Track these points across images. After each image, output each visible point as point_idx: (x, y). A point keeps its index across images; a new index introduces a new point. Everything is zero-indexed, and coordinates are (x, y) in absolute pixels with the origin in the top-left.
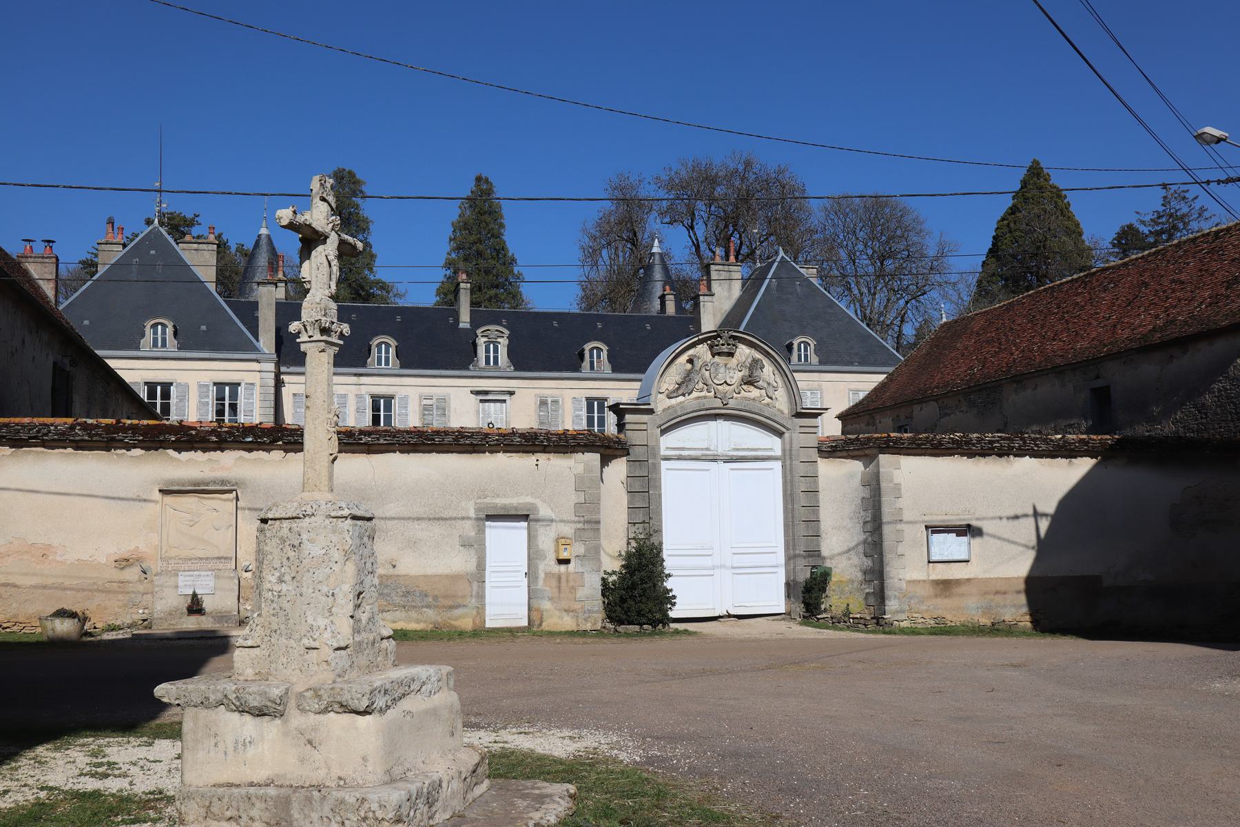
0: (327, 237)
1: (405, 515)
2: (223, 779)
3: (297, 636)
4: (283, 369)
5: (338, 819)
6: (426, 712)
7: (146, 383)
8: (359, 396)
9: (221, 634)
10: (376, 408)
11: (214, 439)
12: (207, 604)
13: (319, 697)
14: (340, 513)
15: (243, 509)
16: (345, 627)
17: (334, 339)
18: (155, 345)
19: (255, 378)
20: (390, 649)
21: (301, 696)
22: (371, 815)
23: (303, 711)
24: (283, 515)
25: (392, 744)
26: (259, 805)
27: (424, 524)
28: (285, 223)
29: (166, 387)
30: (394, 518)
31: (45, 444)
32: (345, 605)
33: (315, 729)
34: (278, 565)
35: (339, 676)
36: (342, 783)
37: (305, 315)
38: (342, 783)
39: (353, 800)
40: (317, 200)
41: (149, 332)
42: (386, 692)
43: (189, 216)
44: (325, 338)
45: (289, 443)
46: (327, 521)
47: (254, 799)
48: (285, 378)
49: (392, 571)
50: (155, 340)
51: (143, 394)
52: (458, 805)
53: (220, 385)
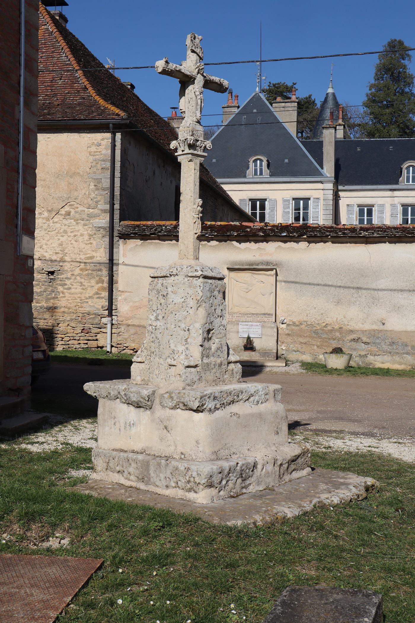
0: (195, 79)
1: (392, 287)
2: (118, 446)
3: (164, 357)
4: (340, 187)
5: (175, 480)
6: (252, 415)
7: (250, 200)
8: (393, 206)
9: (260, 364)
10: (361, 212)
11: (262, 234)
12: (257, 344)
13: (172, 398)
14: (194, 274)
15: (281, 281)
16: (196, 353)
17: (200, 153)
18: (256, 174)
19: (319, 194)
20: (235, 370)
21: (162, 396)
22: (192, 479)
23: (163, 407)
24: (159, 275)
25: (218, 433)
26: (133, 465)
27: (405, 295)
28: (160, 70)
29: (263, 202)
30: (384, 290)
31: (159, 238)
32: (197, 338)
33: (169, 419)
34: (155, 309)
35: (189, 385)
36: (183, 457)
37: (180, 137)
38: (183, 457)
39: (182, 468)
40: (189, 52)
41: (251, 165)
42: (215, 398)
43: (290, 84)
44: (191, 151)
45: (311, 236)
46: (186, 279)
47: (130, 461)
48: (341, 194)
49: (382, 327)
50: (256, 170)
51: (248, 210)
52: (271, 481)
53: (297, 200)
